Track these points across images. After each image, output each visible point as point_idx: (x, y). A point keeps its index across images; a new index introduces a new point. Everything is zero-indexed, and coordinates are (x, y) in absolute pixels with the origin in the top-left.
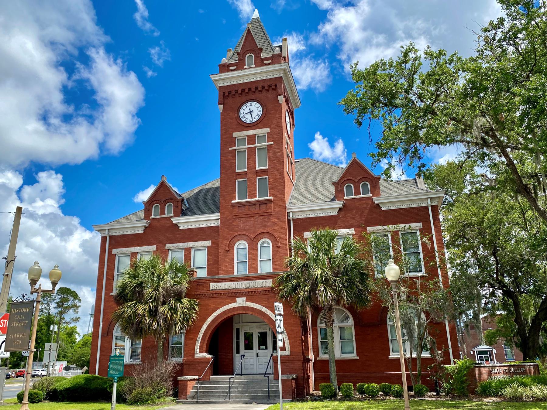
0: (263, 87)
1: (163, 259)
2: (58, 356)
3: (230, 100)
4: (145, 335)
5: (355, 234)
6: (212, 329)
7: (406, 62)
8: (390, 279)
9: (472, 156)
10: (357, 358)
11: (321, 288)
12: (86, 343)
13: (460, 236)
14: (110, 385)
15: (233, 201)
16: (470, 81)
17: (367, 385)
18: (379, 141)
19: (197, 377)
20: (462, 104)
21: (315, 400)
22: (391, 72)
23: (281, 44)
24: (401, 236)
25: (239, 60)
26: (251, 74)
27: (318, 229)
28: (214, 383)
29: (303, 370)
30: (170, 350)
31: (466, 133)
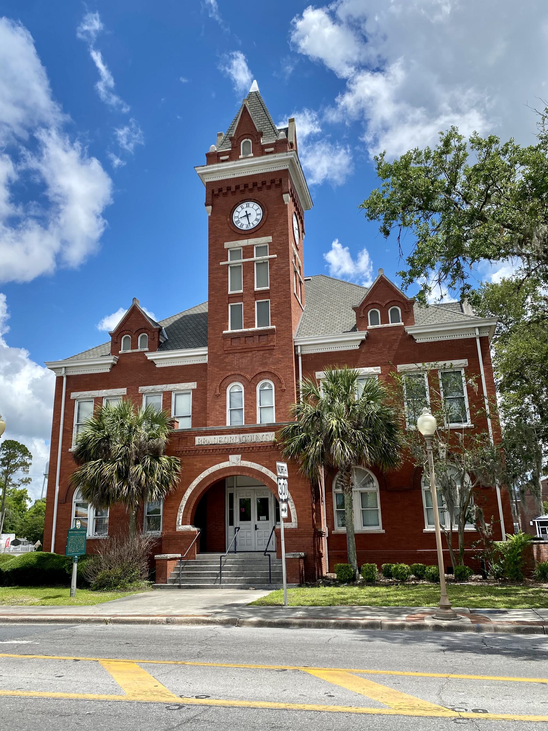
0: (264, 183)
1: (136, 406)
2: (4, 527)
3: (220, 200)
4: (113, 502)
5: (381, 374)
6: (198, 494)
7: (448, 152)
8: (424, 433)
9: (533, 273)
10: (383, 531)
11: (337, 444)
12: (40, 511)
13: (518, 376)
14: (69, 565)
15: (224, 332)
16: (529, 178)
17: (395, 566)
18: (411, 256)
19: (179, 555)
20: (519, 207)
21: (329, 585)
22: (427, 165)
23: (287, 126)
24: (440, 377)
25: (232, 147)
26: (248, 165)
27: (334, 368)
28: (201, 563)
29: (314, 546)
30: (145, 520)
31: (526, 244)
